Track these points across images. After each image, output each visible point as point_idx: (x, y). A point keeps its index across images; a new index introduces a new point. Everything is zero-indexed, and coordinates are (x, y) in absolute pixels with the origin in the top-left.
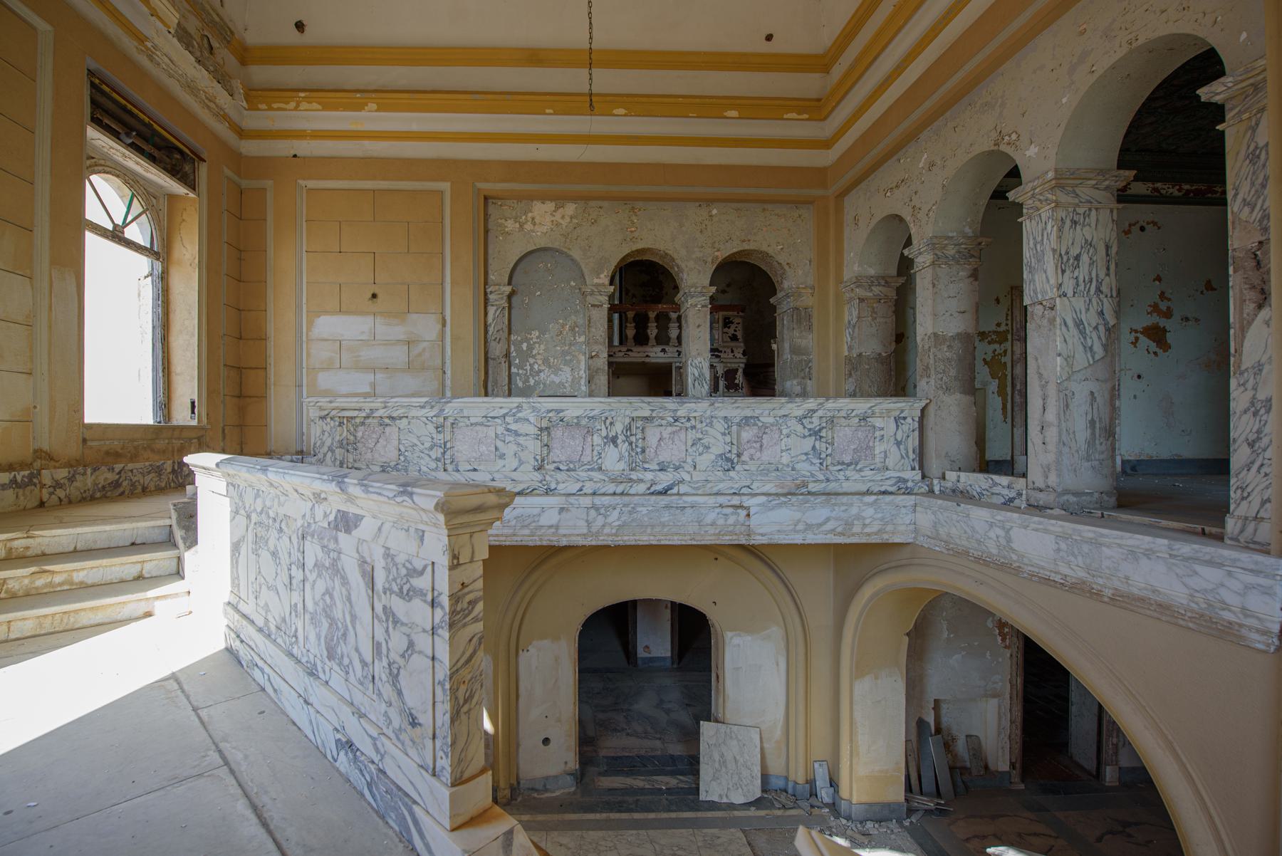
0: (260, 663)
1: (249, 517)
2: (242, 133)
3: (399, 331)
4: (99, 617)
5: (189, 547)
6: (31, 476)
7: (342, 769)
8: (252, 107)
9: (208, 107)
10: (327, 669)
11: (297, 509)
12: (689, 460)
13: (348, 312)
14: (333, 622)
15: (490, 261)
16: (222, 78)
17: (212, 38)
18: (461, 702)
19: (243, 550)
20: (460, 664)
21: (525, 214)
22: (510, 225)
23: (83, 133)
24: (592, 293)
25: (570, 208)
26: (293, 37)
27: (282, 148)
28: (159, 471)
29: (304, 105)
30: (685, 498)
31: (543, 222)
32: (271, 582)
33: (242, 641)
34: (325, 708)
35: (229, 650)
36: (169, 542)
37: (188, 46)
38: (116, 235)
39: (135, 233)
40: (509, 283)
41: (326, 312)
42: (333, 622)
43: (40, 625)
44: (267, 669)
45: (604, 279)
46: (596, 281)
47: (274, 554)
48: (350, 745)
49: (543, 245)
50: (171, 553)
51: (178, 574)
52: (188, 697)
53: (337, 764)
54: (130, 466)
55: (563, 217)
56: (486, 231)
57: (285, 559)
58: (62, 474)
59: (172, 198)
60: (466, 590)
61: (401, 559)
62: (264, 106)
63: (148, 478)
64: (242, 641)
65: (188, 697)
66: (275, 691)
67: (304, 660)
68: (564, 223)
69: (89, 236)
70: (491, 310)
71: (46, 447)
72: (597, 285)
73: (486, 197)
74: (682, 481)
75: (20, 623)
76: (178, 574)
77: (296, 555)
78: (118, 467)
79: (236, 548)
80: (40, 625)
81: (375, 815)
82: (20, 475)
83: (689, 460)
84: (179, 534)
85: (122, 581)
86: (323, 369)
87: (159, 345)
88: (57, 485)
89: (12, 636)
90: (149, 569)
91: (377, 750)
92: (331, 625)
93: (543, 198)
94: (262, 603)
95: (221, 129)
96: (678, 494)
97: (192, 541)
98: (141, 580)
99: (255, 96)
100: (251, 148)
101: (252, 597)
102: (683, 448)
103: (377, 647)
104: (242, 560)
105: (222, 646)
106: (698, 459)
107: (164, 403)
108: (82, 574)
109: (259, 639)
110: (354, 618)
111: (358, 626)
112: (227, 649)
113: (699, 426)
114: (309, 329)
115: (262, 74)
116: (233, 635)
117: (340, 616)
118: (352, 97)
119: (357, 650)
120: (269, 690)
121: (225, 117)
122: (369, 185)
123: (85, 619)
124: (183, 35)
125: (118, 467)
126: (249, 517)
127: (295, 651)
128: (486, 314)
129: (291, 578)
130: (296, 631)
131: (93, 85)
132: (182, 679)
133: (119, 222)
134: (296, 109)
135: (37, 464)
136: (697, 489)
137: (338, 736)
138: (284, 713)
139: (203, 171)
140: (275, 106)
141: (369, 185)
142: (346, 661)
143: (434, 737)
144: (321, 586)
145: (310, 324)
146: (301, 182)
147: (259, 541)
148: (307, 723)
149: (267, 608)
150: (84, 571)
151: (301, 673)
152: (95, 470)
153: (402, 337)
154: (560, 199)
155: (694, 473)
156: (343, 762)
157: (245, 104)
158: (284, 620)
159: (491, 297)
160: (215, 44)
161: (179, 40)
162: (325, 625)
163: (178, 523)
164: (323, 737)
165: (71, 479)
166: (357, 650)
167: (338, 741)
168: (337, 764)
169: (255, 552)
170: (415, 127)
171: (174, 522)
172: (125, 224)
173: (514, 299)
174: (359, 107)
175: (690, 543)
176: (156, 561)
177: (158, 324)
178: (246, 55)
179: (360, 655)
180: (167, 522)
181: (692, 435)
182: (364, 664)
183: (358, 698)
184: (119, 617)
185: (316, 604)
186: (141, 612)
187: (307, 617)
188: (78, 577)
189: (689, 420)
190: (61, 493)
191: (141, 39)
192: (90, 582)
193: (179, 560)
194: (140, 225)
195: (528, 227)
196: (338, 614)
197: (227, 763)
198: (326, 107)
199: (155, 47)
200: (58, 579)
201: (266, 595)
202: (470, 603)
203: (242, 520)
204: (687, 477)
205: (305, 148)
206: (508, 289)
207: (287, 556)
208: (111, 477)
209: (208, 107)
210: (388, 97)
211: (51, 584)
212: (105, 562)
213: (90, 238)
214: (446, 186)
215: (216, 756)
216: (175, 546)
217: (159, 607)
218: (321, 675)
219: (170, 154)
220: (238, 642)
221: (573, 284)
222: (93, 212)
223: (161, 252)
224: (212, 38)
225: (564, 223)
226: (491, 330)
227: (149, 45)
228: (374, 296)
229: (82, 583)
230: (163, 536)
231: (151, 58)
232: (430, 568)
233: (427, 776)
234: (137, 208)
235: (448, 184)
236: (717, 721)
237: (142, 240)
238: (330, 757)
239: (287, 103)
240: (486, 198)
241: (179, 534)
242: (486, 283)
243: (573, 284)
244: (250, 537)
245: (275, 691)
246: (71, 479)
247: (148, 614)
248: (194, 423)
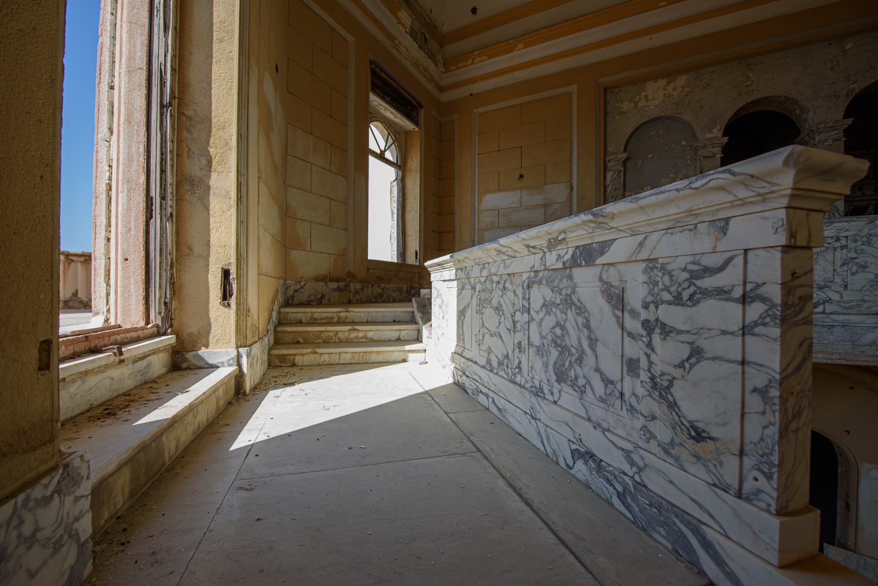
0: (485, 390)
1: (474, 288)
2: (441, 89)
3: (538, 199)
4: (380, 358)
5: (425, 323)
6: (346, 286)
7: (579, 476)
8: (447, 70)
9: (424, 75)
10: (556, 391)
11: (525, 263)
12: (838, 279)
13: (504, 190)
14: (563, 349)
15: (608, 137)
16: (431, 56)
17: (427, 32)
18: (790, 416)
19: (468, 313)
20: (790, 370)
21: (639, 94)
22: (625, 106)
23: (368, 97)
24: (705, 146)
25: (682, 80)
26: (470, 19)
27: (463, 92)
28: (400, 290)
29: (477, 59)
30: (835, 317)
31: (656, 97)
32: (493, 329)
33: (468, 377)
34: (558, 422)
35: (457, 384)
36: (413, 321)
37: (415, 39)
38: (381, 157)
39: (388, 155)
40: (625, 151)
41: (490, 192)
42: (563, 349)
43: (353, 357)
44: (491, 394)
45: (717, 132)
46: (708, 136)
47: (498, 309)
48: (588, 456)
49: (656, 116)
50: (414, 327)
51: (419, 339)
52: (439, 405)
53: (573, 472)
54: (388, 286)
55: (675, 89)
56: (606, 115)
57: (508, 309)
58: (358, 286)
59: (407, 133)
60: (798, 282)
61: (675, 265)
62: (454, 68)
63: (396, 294)
64: (468, 377)
65: (439, 405)
66: (499, 410)
67: (528, 386)
68: (675, 93)
69: (371, 159)
70: (609, 175)
71: (352, 271)
72: (709, 139)
73: (604, 88)
74: (830, 300)
75: (344, 355)
76: (419, 339)
77: (520, 302)
78: (383, 285)
79: (461, 314)
80: (353, 357)
81: (633, 526)
82: (342, 284)
83: (838, 279)
84: (418, 316)
85: (390, 341)
86: (487, 229)
87: (400, 219)
88: (356, 292)
89: (341, 362)
90: (404, 335)
91: (632, 463)
92: (561, 353)
93: (655, 77)
94: (484, 347)
95: (431, 87)
96: (824, 312)
97: (427, 318)
98: (399, 341)
99: (449, 64)
100: (446, 97)
101: (475, 345)
102: (830, 268)
103: (632, 366)
104: (467, 321)
105: (451, 381)
106: (850, 279)
107: (402, 251)
108: (372, 333)
109: (484, 374)
110: (593, 342)
111: (600, 348)
112: (454, 383)
113: (851, 245)
114: (479, 204)
115: (452, 49)
116: (460, 373)
117: (575, 342)
118: (506, 46)
119: (597, 370)
120: (494, 409)
121: (431, 80)
122: (518, 101)
123: (374, 358)
124: (413, 33)
125: (383, 285)
126: (474, 288)
127: (518, 379)
128: (605, 178)
129: (514, 322)
130: (520, 362)
131: (373, 72)
132: (433, 395)
133: (383, 149)
134: (472, 64)
135: (348, 280)
136: (850, 308)
137: (574, 447)
138: (509, 426)
139: (422, 112)
140: (460, 65)
141: (518, 101)
142: (581, 382)
143: (742, 453)
144: (550, 321)
145: (480, 200)
146: (475, 110)
147: (482, 303)
148: (535, 435)
149: (490, 351)
150: (373, 332)
151: (527, 395)
152: (372, 286)
153: (541, 202)
154: (671, 75)
155: (845, 293)
156: (581, 469)
157: (443, 70)
158: (507, 356)
159: (609, 164)
160: (428, 37)
161: (411, 36)
162: (555, 353)
163: (418, 309)
164: (555, 446)
165: (362, 290)
166: (597, 370)
167: (573, 452)
168: (573, 472)
169: (480, 312)
170: (550, 52)
171: (415, 309)
172: (385, 150)
173: (628, 165)
174: (512, 50)
175: (838, 362)
176: (407, 330)
177: (400, 207)
178: (444, 40)
179: (602, 374)
180: (411, 309)
181: (840, 255)
182: (607, 382)
183: (598, 413)
184: (390, 360)
185: (543, 337)
186: (400, 359)
187: (532, 351)
188: (370, 335)
189: (838, 239)
190: (358, 297)
191: (392, 38)
192: (375, 338)
193: (419, 332)
194: (391, 152)
195: (642, 103)
196: (572, 340)
197: (479, 451)
198: (491, 56)
199: (400, 43)
200: (361, 335)
201: (489, 341)
202: (801, 298)
203: (468, 292)
204: (835, 297)
205: (476, 88)
206: (624, 156)
207: (510, 306)
208: (379, 291)
209: (424, 75)
210: (530, 38)
211: (357, 337)
212: (382, 327)
213: (371, 159)
214: (573, 88)
215: (469, 444)
216: (416, 323)
217: (411, 356)
218: (548, 396)
219: (406, 105)
220: (464, 378)
221: (684, 143)
222: (372, 146)
223: (401, 166)
224: (427, 32)
225: (675, 93)
226: (609, 190)
227: (397, 42)
228: (521, 176)
229: (371, 338)
230: (407, 317)
231: (398, 50)
232: (739, 260)
233: (729, 498)
234: (390, 141)
235: (576, 86)
236: (844, 547)
237: (391, 159)
238: (562, 464)
239: (467, 61)
240: (605, 89)
241: (418, 316)
242: (605, 154)
243: (684, 143)
244: (475, 302)
245: (499, 410)
246: (362, 290)
247: (404, 361)
248: (417, 264)
